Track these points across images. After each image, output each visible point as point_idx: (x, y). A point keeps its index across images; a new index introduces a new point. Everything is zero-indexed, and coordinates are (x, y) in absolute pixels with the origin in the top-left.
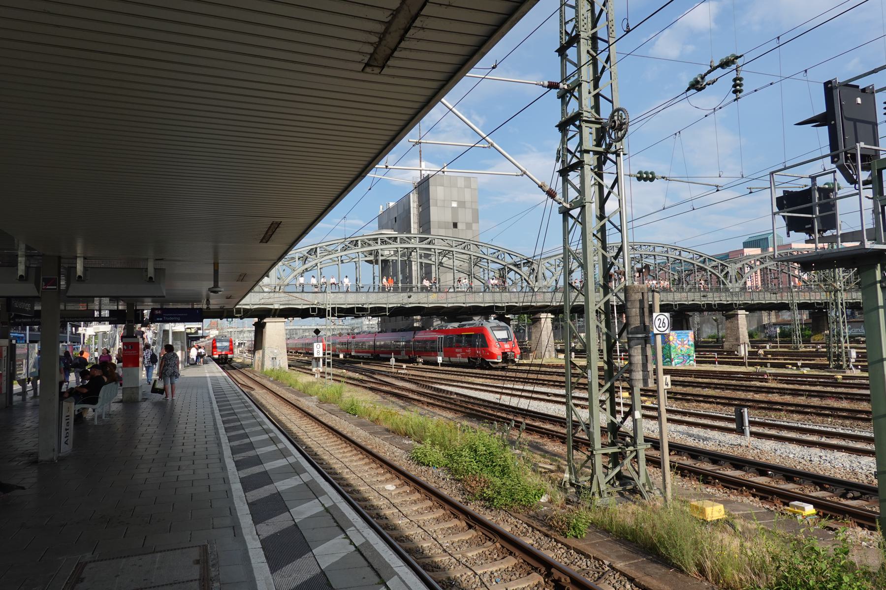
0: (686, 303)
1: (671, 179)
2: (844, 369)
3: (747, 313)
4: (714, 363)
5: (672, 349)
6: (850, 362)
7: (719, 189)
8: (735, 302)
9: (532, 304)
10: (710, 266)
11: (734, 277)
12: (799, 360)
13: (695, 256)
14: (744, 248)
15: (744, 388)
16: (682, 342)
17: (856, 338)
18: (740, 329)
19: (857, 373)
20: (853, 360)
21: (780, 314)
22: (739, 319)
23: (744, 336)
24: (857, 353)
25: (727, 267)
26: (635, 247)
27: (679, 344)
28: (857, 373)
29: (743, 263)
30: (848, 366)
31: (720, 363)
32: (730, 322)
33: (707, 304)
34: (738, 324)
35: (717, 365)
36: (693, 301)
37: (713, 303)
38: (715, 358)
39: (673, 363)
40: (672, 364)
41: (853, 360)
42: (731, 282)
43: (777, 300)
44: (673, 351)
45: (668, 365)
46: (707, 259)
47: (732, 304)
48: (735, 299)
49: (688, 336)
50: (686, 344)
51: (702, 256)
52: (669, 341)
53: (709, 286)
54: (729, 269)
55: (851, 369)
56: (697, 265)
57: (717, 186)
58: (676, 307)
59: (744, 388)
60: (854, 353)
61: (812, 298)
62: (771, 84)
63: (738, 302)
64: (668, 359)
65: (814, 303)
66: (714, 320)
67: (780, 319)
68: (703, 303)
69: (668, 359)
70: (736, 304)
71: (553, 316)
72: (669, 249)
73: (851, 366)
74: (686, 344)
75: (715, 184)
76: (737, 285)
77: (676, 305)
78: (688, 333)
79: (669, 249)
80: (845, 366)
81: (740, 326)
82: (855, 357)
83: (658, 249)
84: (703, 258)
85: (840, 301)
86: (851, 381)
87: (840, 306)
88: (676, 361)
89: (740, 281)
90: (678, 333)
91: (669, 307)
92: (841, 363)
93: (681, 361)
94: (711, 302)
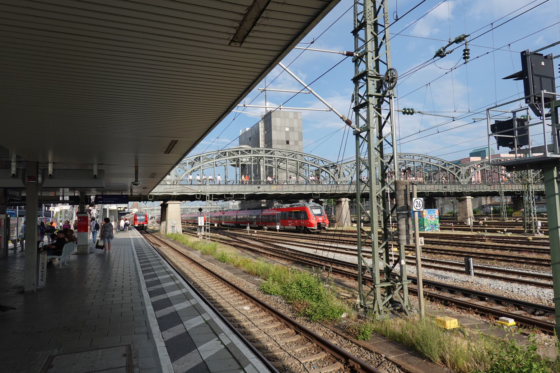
0: (434, 191)
2: (534, 233)
3: (472, 198)
4: (451, 229)
5: (425, 221)
6: (537, 229)
7: (455, 119)
8: (465, 191)
10: (449, 168)
11: (464, 175)
12: (505, 227)
13: (439, 162)
15: (470, 245)
16: (431, 216)
18: (468, 208)
19: (542, 236)
20: (539, 228)
22: (467, 202)
23: (470, 213)
24: (542, 223)
26: (402, 156)
27: (429, 218)
29: (469, 166)
30: (536, 231)
31: (455, 229)
32: (461, 204)
34: (466, 205)
35: (453, 231)
36: (438, 190)
37: (451, 191)
38: (452, 226)
39: (426, 229)
40: (424, 230)
41: (539, 228)
42: (462, 178)
43: (491, 190)
44: (425, 222)
45: (422, 231)
46: (447, 164)
47: (463, 192)
48: (464, 189)
49: (435, 212)
50: (434, 218)
51: (444, 162)
52: (423, 215)
54: (461, 170)
55: (538, 233)
56: (441, 168)
57: (453, 118)
58: (427, 194)
59: (470, 245)
61: (513, 189)
62: (487, 53)
63: (466, 191)
64: (422, 227)
65: (514, 191)
68: (444, 191)
69: (422, 227)
70: (465, 192)
72: (423, 157)
73: (538, 231)
75: (452, 117)
76: (466, 180)
77: (427, 193)
78: (435, 211)
79: (423, 157)
80: (534, 231)
81: (468, 206)
82: (541, 226)
83: (416, 158)
84: (445, 163)
86: (538, 241)
88: (427, 228)
89: (467, 178)
90: (429, 211)
91: (423, 194)
92: (532, 229)
93: (430, 228)
94: (449, 191)
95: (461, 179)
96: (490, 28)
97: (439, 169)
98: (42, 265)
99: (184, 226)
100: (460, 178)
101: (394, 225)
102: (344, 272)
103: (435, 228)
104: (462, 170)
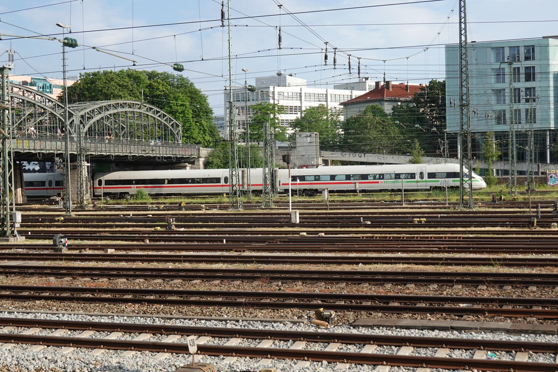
1: (99, 50)
2: (8, 237)
6: (15, 227)
7: (135, 63)
9: (103, 153)
12: (299, 184)
17: (51, 198)
19: (21, 240)
20: (17, 225)
24: (22, 216)
28: (21, 240)
30: (13, 232)
41: (17, 225)
43: (123, 153)
55: (15, 236)
57: (134, 62)
60: (19, 217)
61: (132, 151)
62: (247, 26)
65: (155, 156)
71: (89, 164)
73: (16, 233)
75: (132, 60)
80: (9, 232)
82: (20, 221)
85: (7, 151)
86: (7, 251)
87: (7, 158)
92: (5, 229)
96: (326, 83)
98: (421, 174)
100: (73, 130)
102: (89, 217)
104: (75, 117)
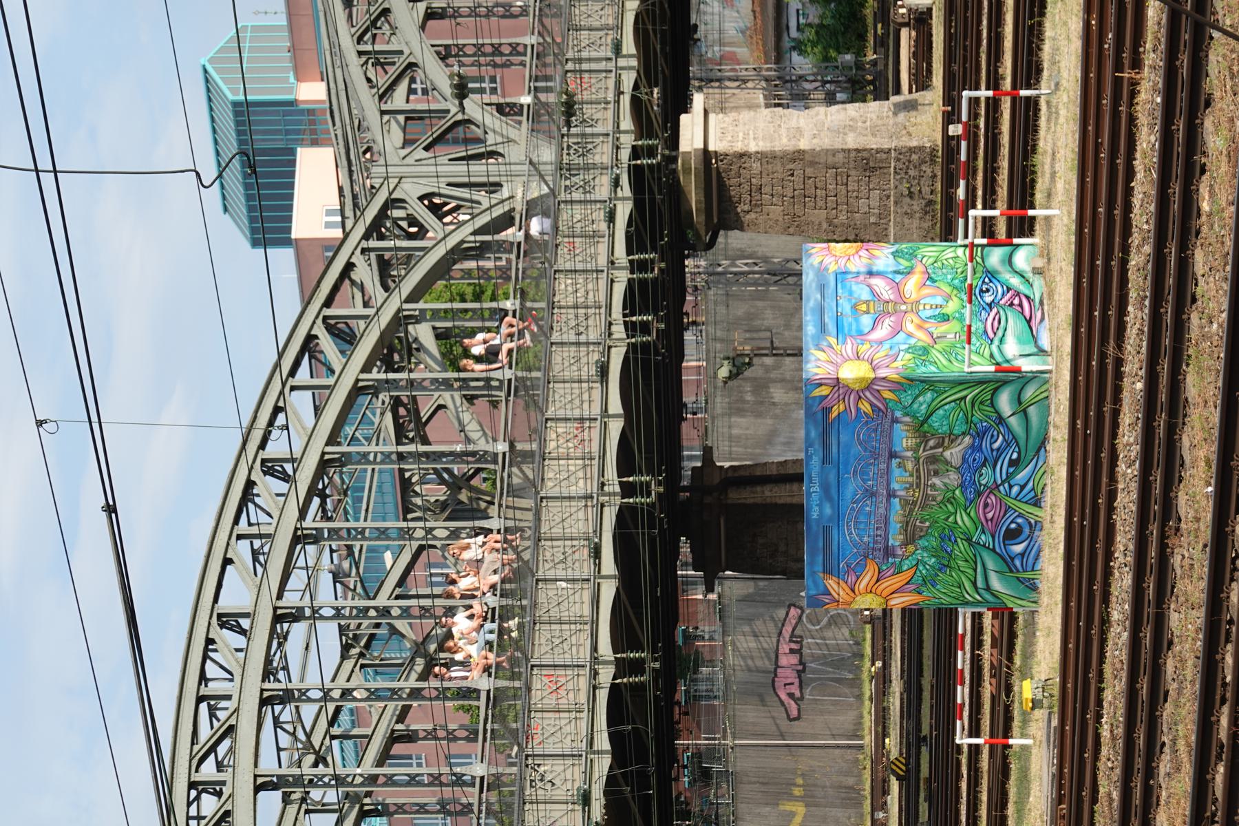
0: (609, 591)
3: (698, 100)
4: (1027, 114)
5: (929, 370)
8: (625, 155)
10: (380, 294)
11: (461, 168)
13: (303, 375)
14: (287, 242)
15: (1157, 477)
16: (884, 310)
18: (804, 145)
21: (714, 52)
22: (739, 147)
23: (841, 130)
25: (391, 203)
26: (205, 732)
27: (898, 329)
29: (373, 118)
31: (1029, 70)
32: (756, 206)
33: (630, 305)
34: (766, 157)
35: (1044, 89)
36: (596, 553)
37: (622, 277)
38: (993, 106)
39: (1028, 365)
40: (1035, 376)
42: (493, 187)
43: (595, 660)
44: (941, 366)
45: (1044, 402)
46: (327, 312)
47: (637, 174)
48: (602, 154)
49: (841, 275)
50: (897, 287)
51: (310, 338)
52: (870, 385)
53: (508, 305)
54: (411, 191)
56: (366, 368)
58: (645, 328)
59: (1157, 477)
63: (628, 141)
64: (1005, 402)
66: (732, 376)
67: (743, 52)
68: (619, 331)
69: (1005, 402)
70: (636, 153)
72: (243, 527)
74: (897, 287)
76: (515, 153)
77: (627, 490)
78: (821, 271)
79: (243, 527)
81: (783, 143)
83: (236, 596)
84: (320, 330)
88: (1012, 348)
89: (491, 138)
90: (823, 329)
91: (642, 535)
93: (1014, 323)
94: (619, 290)
95: (505, 193)
97: (374, 390)
99: (1126, 62)
101: (975, 731)
103: (1015, 281)
